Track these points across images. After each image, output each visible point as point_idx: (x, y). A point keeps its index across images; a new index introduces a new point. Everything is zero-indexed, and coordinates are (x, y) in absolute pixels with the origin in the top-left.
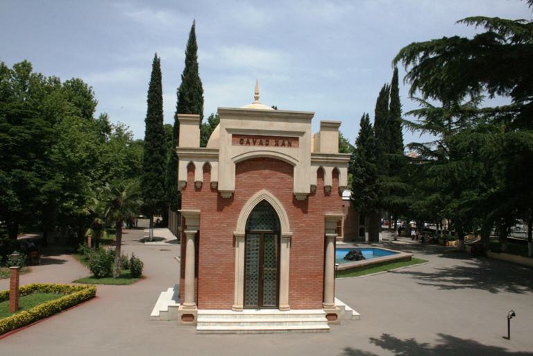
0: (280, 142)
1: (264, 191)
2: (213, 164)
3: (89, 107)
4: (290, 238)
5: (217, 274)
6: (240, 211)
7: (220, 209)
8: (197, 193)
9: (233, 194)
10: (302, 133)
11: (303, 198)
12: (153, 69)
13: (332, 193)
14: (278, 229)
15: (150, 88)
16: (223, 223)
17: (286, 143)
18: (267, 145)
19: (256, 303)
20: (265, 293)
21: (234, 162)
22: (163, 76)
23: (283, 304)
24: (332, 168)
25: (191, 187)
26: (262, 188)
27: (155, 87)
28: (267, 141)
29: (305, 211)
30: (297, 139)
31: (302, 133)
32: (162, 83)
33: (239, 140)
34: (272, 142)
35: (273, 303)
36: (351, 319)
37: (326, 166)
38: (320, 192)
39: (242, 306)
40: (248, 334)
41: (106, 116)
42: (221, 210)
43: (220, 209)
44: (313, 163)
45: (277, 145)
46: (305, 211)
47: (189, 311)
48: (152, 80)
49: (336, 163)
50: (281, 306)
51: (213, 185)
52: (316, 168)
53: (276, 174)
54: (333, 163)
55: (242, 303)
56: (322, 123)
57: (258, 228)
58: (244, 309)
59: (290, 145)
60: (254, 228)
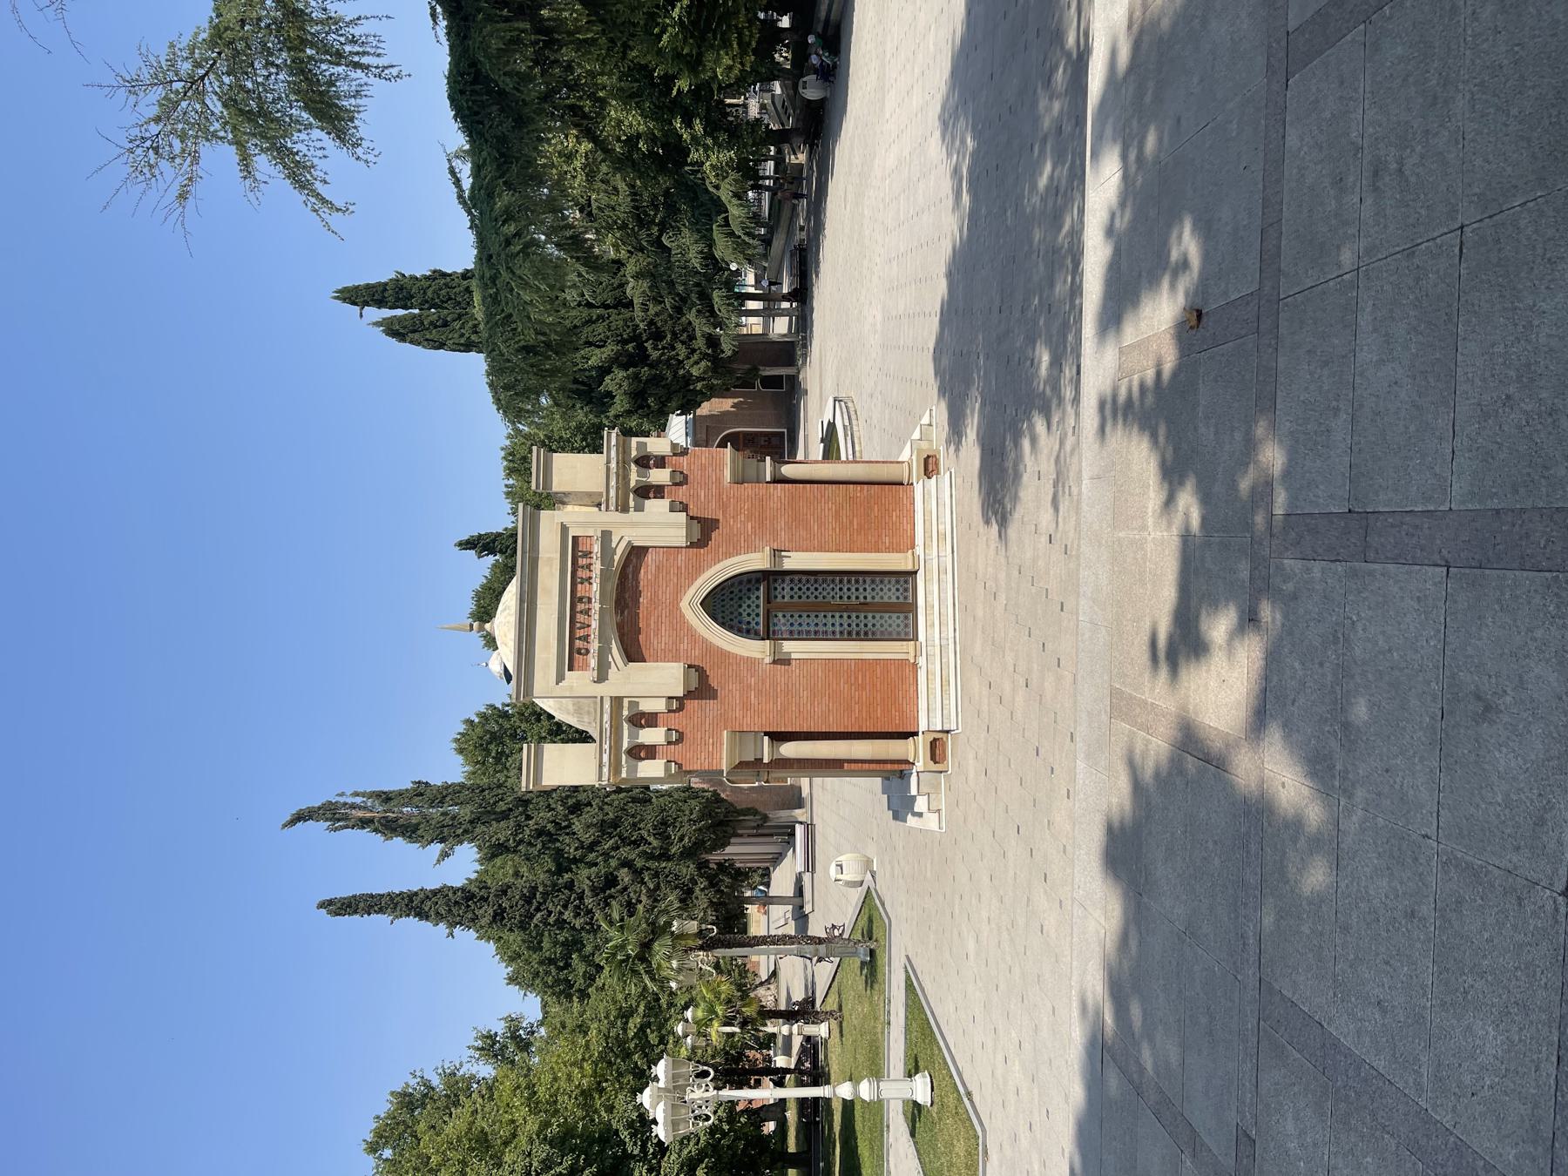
1: (684, 605)
4: (776, 553)
28: (581, 599)
50: (909, 568)
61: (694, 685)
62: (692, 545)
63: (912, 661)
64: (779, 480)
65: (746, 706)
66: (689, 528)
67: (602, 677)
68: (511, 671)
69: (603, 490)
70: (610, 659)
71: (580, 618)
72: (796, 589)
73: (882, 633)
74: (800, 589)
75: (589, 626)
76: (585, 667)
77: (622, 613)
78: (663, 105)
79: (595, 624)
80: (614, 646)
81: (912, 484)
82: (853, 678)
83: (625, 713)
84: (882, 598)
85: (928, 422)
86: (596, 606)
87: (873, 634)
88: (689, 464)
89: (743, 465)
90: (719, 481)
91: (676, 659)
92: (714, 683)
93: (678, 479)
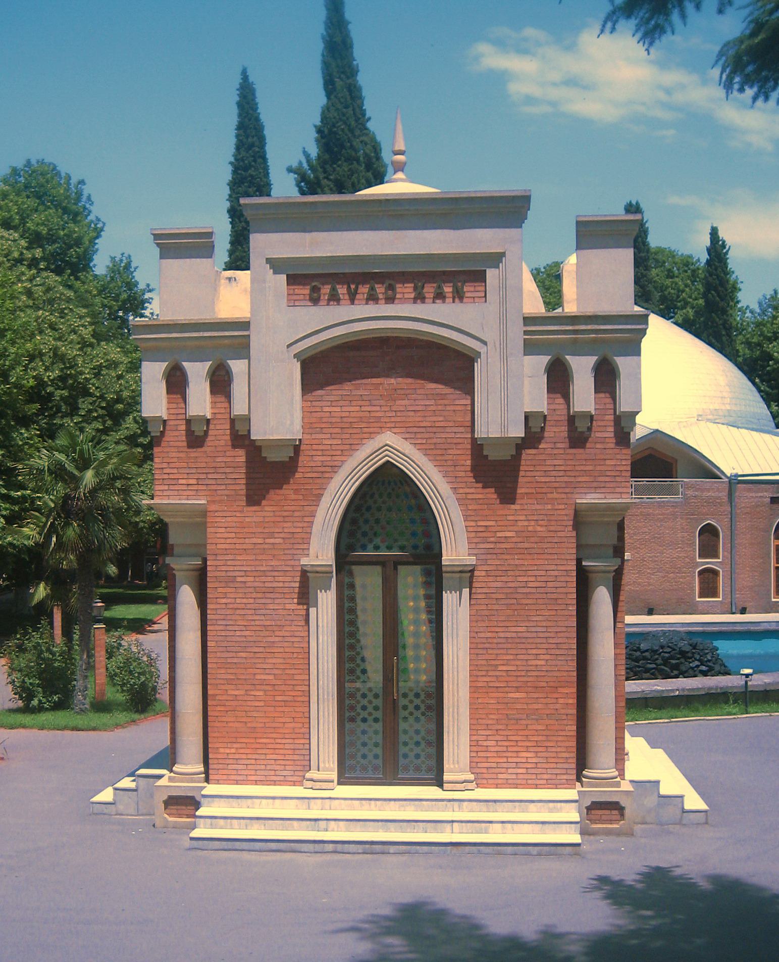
0: (429, 290)
1: (388, 438)
2: (237, 366)
3: (78, 242)
4: (467, 576)
5: (262, 683)
6: (319, 497)
7: (254, 497)
8: (195, 453)
9: (297, 449)
10: (496, 259)
11: (506, 454)
12: (240, 115)
13: (596, 435)
14: (436, 551)
15: (235, 172)
16: (271, 535)
17: (448, 289)
18: (390, 300)
19: (376, 768)
20: (403, 738)
21: (295, 356)
22: (268, 133)
23: (451, 771)
24: (592, 360)
25: (176, 436)
26: (381, 429)
27: (246, 169)
28: (391, 288)
29: (508, 496)
30: (479, 277)
31: (496, 259)
32: (269, 156)
33: (306, 291)
34: (406, 290)
35: (429, 770)
36: (680, 823)
37: (573, 354)
38: (556, 432)
39: (334, 776)
40: (335, 852)
41: (128, 266)
42: (258, 503)
43: (254, 497)
44: (530, 348)
45: (420, 298)
46: (508, 496)
47: (182, 787)
48: (238, 148)
49: (603, 341)
50: (447, 777)
51: (194, 428)
52: (544, 360)
53: (443, 396)
54: (594, 341)
55: (334, 765)
56: (579, 224)
57: (377, 548)
58: (340, 783)
59: (459, 296)
60: (364, 548)
61: (272, 456)
62: (477, 447)
63: (308, 775)
66: (502, 442)
72: (364, 714)
73: (352, 732)
74: (364, 708)
78: (124, 302)
84: (405, 744)
87: (352, 720)
88: (603, 441)
89: (608, 523)
91: (307, 426)
93: (581, 426)
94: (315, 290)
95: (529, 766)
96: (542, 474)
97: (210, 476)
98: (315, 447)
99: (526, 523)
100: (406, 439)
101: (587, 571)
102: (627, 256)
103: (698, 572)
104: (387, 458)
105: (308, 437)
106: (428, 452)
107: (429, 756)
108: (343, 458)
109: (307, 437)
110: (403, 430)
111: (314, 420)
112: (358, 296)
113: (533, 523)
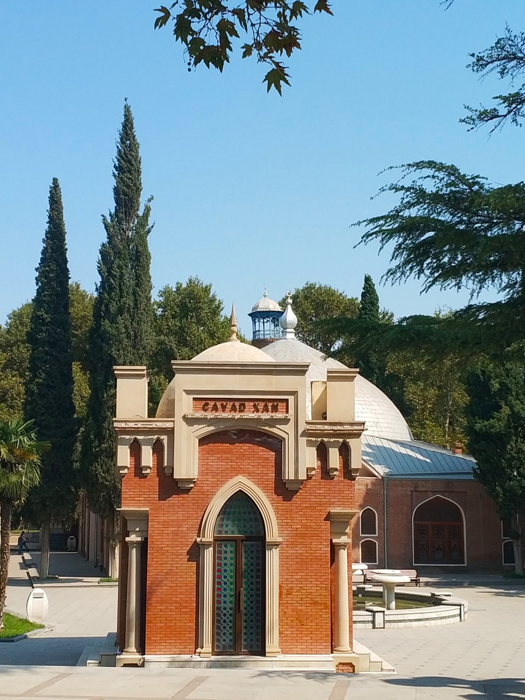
64: (334, 549)
65: (166, 524)
67: (190, 421)
68: (192, 360)
69: (328, 421)
70: (205, 425)
71: (229, 405)
75: (224, 411)
76: (195, 408)
77: (234, 434)
79: (225, 415)
80: (212, 428)
81: (332, 653)
82: (185, 604)
83: (326, 440)
85: (384, 668)
86: (237, 416)
90: (331, 504)
91: (201, 473)
92: (174, 499)
94: (207, 404)
95: (253, 458)
96: (314, 497)
97: (151, 496)
98: (204, 482)
99: (306, 521)
100: (248, 479)
101: (334, 545)
102: (306, 479)
103: (362, 543)
104: (240, 489)
105: (201, 477)
106: (260, 485)
107: (257, 640)
108: (218, 488)
109: (200, 477)
110: (247, 474)
111: (204, 469)
112: (226, 409)
113: (309, 521)
